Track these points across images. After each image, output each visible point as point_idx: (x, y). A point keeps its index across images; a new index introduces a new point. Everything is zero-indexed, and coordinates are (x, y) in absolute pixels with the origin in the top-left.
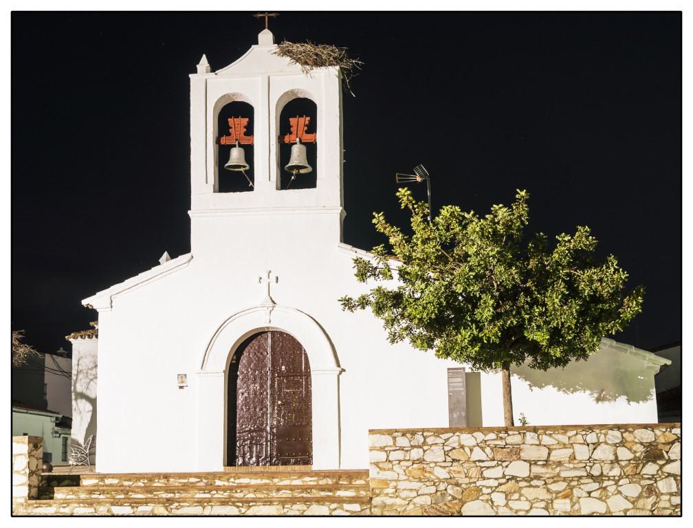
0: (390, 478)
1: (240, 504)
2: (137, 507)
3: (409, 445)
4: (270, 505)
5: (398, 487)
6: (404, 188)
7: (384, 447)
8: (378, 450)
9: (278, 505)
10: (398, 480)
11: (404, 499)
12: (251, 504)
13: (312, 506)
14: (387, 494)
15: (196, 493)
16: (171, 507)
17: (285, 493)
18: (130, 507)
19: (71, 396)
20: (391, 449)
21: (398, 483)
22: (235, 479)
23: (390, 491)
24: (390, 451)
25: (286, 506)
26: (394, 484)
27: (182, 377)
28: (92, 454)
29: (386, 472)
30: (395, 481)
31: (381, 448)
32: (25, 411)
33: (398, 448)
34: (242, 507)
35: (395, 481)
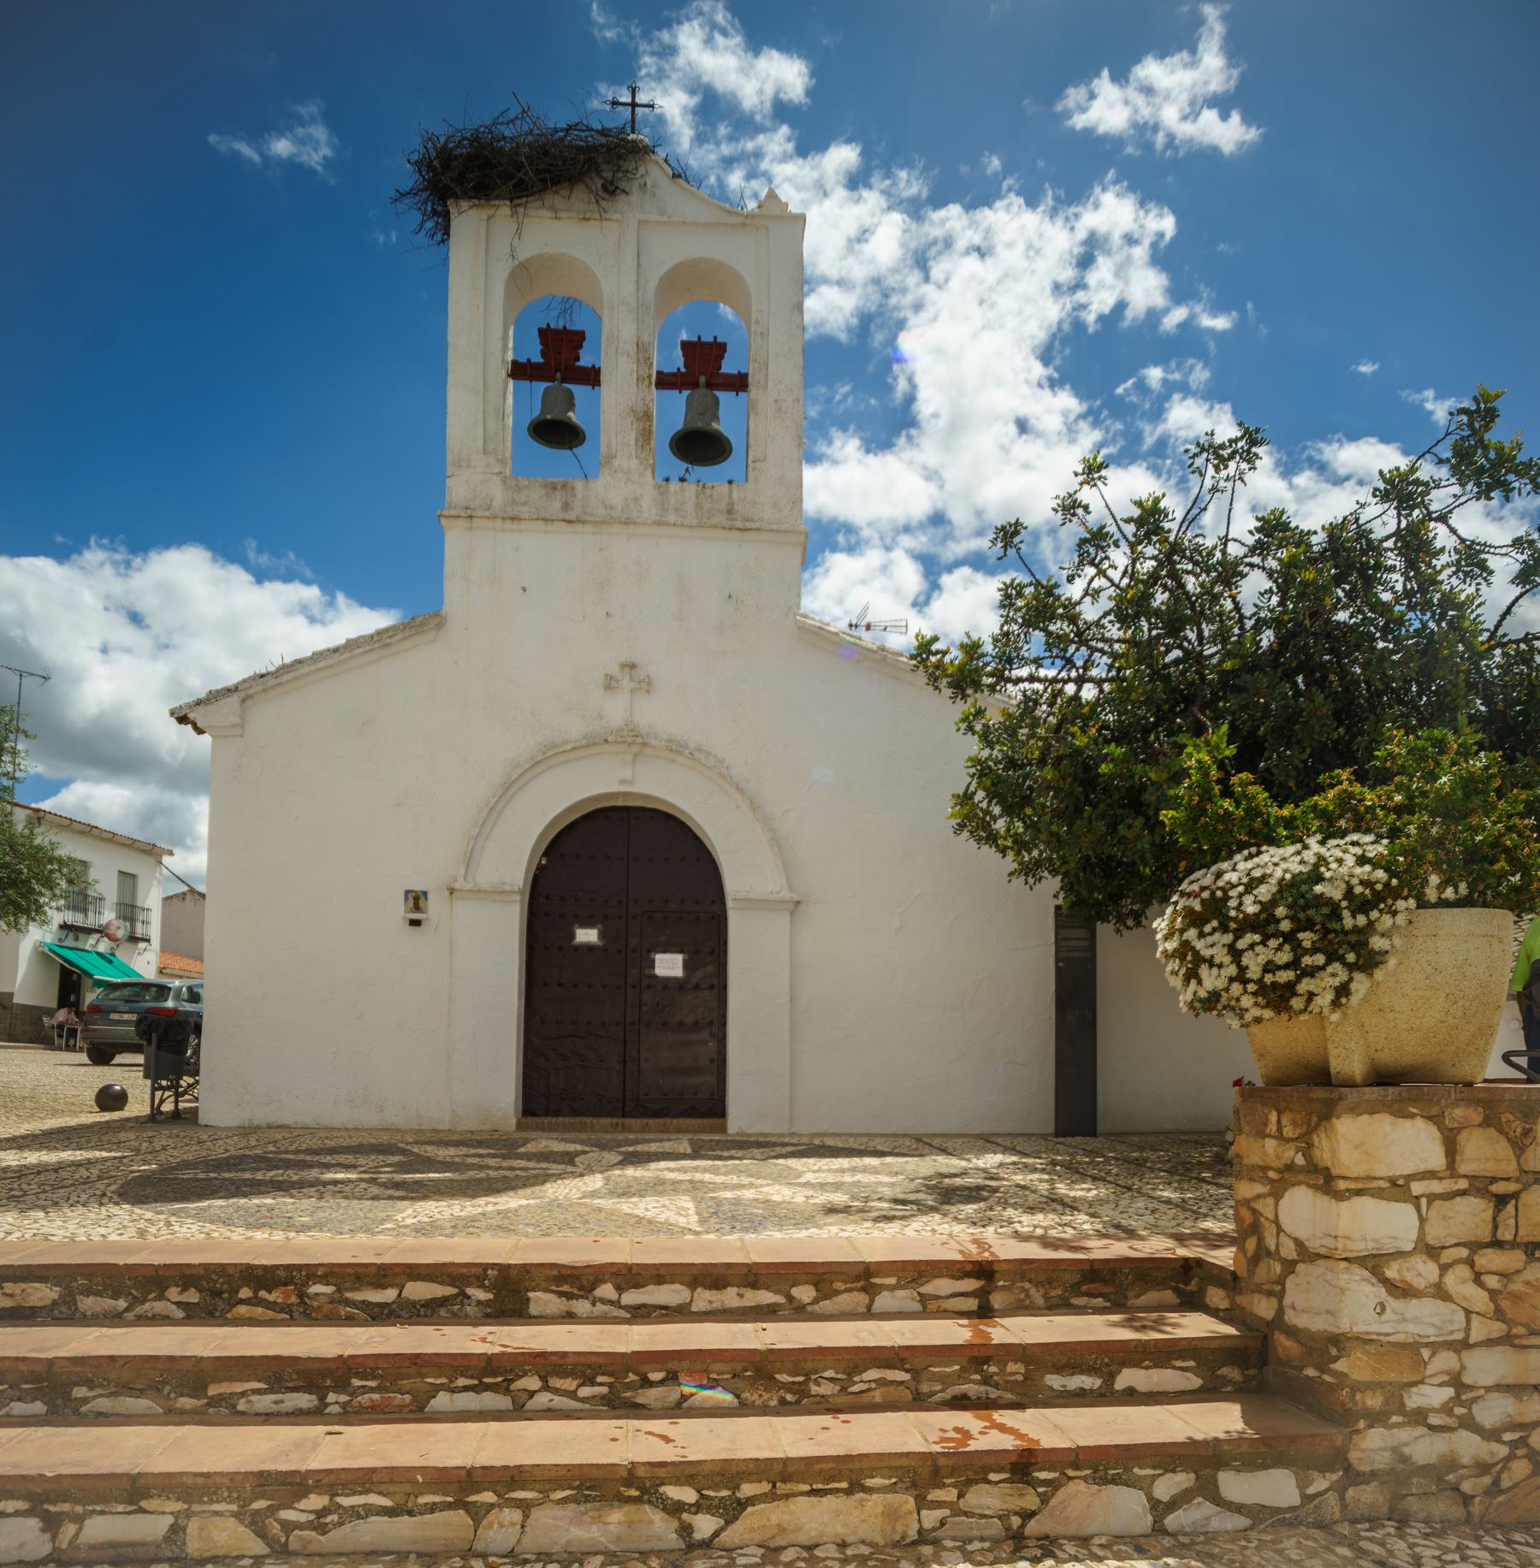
0: (1431, 1334)
1: (688, 1495)
2: (79, 1520)
3: (1511, 1168)
4: (849, 1492)
5: (1467, 1379)
6: (1431, 413)
7: (1411, 1177)
8: (1378, 1194)
9: (892, 1489)
10: (1462, 1346)
11: (1492, 1435)
12: (747, 1490)
13: (1061, 1494)
14: (1419, 1417)
15: (435, 1390)
16: (287, 1515)
17: (881, 1382)
18: (34, 1523)
19: (1125, 381)
20: (1436, 1187)
21: (1465, 1354)
22: (620, 1289)
23: (1433, 1396)
24: (1432, 1198)
25: (936, 1495)
26: (1446, 1361)
27: (416, 900)
28: (398, 1553)
29: (1414, 1307)
30: (1450, 1346)
31: (1393, 1182)
32: (120, 1550)
33: (1463, 1184)
34: (697, 1508)
35: (1450, 1346)
